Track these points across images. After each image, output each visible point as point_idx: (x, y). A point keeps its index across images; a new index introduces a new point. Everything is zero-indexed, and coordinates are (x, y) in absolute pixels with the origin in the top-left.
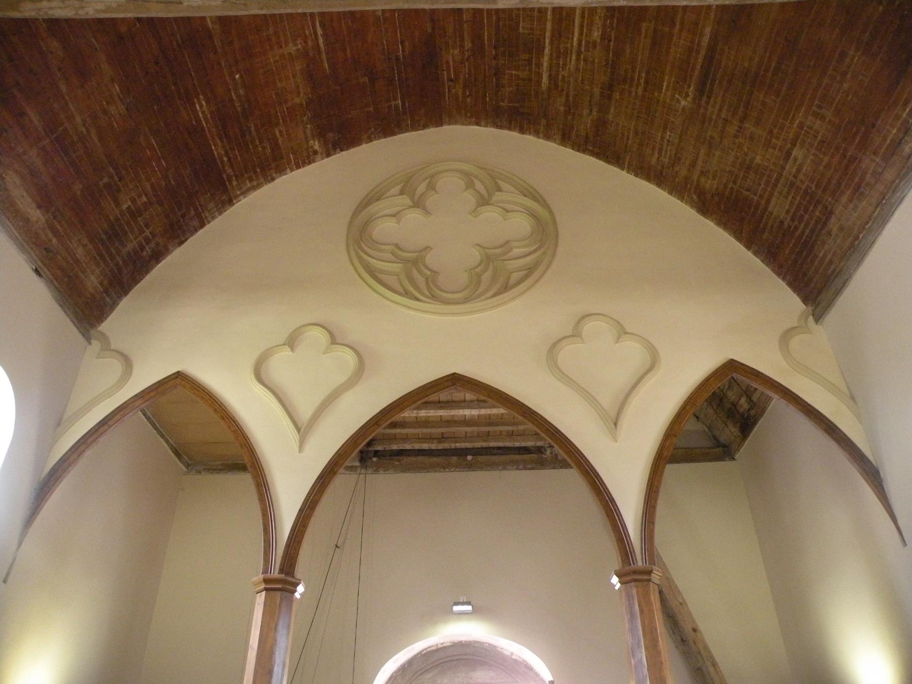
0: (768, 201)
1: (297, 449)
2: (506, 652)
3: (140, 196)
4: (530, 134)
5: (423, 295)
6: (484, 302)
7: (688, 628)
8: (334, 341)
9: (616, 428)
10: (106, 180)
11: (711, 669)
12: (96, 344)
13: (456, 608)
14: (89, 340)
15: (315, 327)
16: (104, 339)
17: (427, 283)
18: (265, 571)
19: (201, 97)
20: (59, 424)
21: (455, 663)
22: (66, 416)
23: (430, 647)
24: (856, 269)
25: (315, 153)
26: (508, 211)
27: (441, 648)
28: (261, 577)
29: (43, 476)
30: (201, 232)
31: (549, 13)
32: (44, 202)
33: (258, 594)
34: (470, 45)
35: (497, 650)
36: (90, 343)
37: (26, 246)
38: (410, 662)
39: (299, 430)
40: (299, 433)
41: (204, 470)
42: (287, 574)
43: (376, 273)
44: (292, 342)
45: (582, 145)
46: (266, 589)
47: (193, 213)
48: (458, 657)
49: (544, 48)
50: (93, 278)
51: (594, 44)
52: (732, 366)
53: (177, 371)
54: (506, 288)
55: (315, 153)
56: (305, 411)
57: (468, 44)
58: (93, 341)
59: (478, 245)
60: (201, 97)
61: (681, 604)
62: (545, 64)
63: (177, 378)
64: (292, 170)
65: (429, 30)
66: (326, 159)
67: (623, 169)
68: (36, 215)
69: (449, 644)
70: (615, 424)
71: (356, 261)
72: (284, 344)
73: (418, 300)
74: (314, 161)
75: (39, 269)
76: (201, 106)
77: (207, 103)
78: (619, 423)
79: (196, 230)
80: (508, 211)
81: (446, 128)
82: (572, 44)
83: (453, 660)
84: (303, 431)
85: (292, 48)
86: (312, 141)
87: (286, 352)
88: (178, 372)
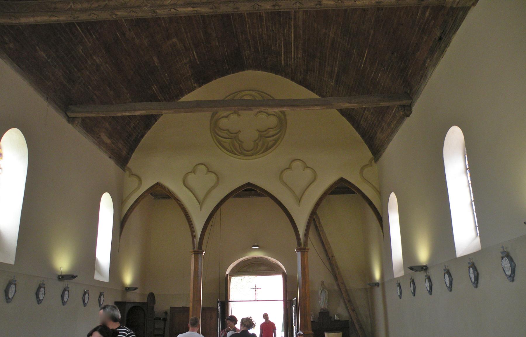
0: (361, 120)
1: (199, 209)
2: (271, 261)
3: (136, 121)
4: (279, 75)
5: (237, 151)
6: (260, 155)
7: (330, 256)
8: (209, 171)
9: (300, 202)
10: (126, 121)
11: (336, 269)
12: (127, 172)
13: (253, 248)
14: (124, 170)
15: (200, 165)
16: (130, 170)
17: (239, 147)
18: (194, 249)
19: (154, 85)
20: (122, 203)
21: (253, 264)
22: (123, 201)
23: (245, 259)
24: (384, 152)
25: (195, 87)
26: (269, 115)
27: (249, 259)
28: (192, 250)
29: (121, 220)
30: (156, 123)
31: (282, 46)
32: (110, 137)
33: (192, 255)
34: (253, 50)
35: (268, 260)
36: (125, 172)
37: (107, 152)
38: (239, 264)
39: (199, 203)
40: (200, 204)
41: (161, 198)
42: (200, 249)
43: (222, 143)
44: (194, 171)
45: (299, 83)
46: (195, 254)
47: (153, 119)
48: (255, 262)
49: (282, 55)
50: (124, 152)
51: (300, 58)
52: (342, 180)
53: (157, 182)
54: (267, 149)
55: (195, 87)
56: (201, 197)
57: (252, 50)
58: (126, 171)
59: (257, 130)
60: (154, 85)
61: (329, 248)
62: (283, 59)
63: (157, 185)
64: (187, 94)
65: (237, 46)
66: (200, 88)
67: (314, 93)
68: (108, 141)
69: (251, 258)
70: (300, 201)
71: (213, 136)
72: (191, 172)
73: (236, 154)
74: (195, 90)
75: (111, 156)
76: (154, 87)
77: (156, 85)
78: (301, 201)
79: (154, 123)
80: (269, 115)
81: (246, 71)
82: (292, 56)
83: (253, 263)
84: (201, 203)
85: (185, 61)
86: (194, 85)
87: (192, 175)
88: (157, 183)
